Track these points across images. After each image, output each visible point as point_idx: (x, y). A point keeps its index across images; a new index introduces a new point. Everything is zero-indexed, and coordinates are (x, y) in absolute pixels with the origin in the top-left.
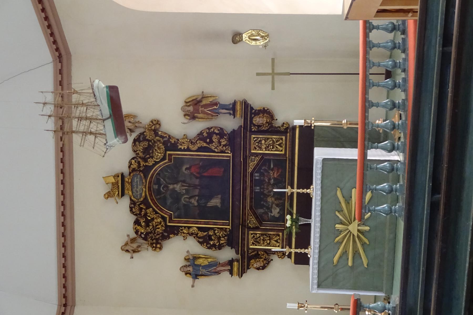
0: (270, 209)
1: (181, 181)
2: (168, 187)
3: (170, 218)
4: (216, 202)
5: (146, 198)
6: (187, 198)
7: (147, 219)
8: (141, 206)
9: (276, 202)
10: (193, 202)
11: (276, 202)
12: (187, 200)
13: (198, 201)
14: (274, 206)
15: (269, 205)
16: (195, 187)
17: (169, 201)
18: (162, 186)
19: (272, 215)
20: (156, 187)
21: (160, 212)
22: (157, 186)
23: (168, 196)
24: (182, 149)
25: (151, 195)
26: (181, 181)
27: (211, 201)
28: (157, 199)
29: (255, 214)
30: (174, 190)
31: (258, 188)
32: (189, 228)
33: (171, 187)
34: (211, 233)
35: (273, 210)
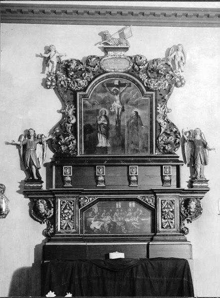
0: (99, 218)
1: (123, 107)
2: (117, 94)
3: (84, 96)
4: (102, 142)
5: (105, 72)
6: (106, 113)
7: (84, 72)
8: (97, 66)
9: (106, 225)
10: (101, 119)
11: (106, 225)
12: (103, 114)
13: (102, 124)
14: (102, 223)
15: (102, 218)
16: (118, 121)
17: (102, 96)
18: (117, 89)
19: (92, 222)
20: (116, 83)
21: (90, 86)
22: (118, 84)
23: (106, 95)
24: (158, 108)
25: (108, 77)
26: (123, 107)
27: (103, 137)
28: (103, 84)
29: (93, 203)
30: (114, 100)
31: (120, 206)
32: (75, 115)
33: (117, 97)
34: (71, 137)
35: (97, 222)
